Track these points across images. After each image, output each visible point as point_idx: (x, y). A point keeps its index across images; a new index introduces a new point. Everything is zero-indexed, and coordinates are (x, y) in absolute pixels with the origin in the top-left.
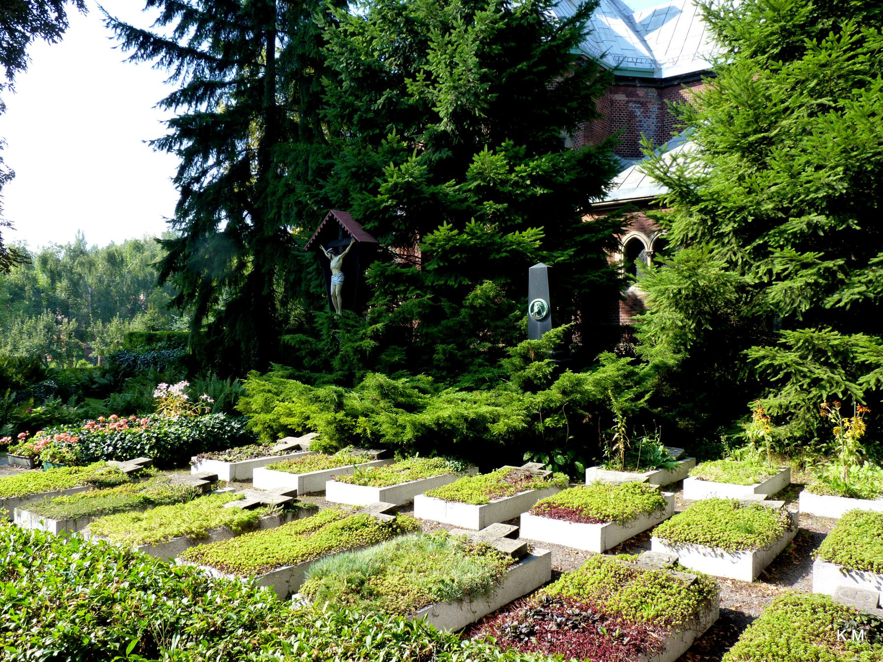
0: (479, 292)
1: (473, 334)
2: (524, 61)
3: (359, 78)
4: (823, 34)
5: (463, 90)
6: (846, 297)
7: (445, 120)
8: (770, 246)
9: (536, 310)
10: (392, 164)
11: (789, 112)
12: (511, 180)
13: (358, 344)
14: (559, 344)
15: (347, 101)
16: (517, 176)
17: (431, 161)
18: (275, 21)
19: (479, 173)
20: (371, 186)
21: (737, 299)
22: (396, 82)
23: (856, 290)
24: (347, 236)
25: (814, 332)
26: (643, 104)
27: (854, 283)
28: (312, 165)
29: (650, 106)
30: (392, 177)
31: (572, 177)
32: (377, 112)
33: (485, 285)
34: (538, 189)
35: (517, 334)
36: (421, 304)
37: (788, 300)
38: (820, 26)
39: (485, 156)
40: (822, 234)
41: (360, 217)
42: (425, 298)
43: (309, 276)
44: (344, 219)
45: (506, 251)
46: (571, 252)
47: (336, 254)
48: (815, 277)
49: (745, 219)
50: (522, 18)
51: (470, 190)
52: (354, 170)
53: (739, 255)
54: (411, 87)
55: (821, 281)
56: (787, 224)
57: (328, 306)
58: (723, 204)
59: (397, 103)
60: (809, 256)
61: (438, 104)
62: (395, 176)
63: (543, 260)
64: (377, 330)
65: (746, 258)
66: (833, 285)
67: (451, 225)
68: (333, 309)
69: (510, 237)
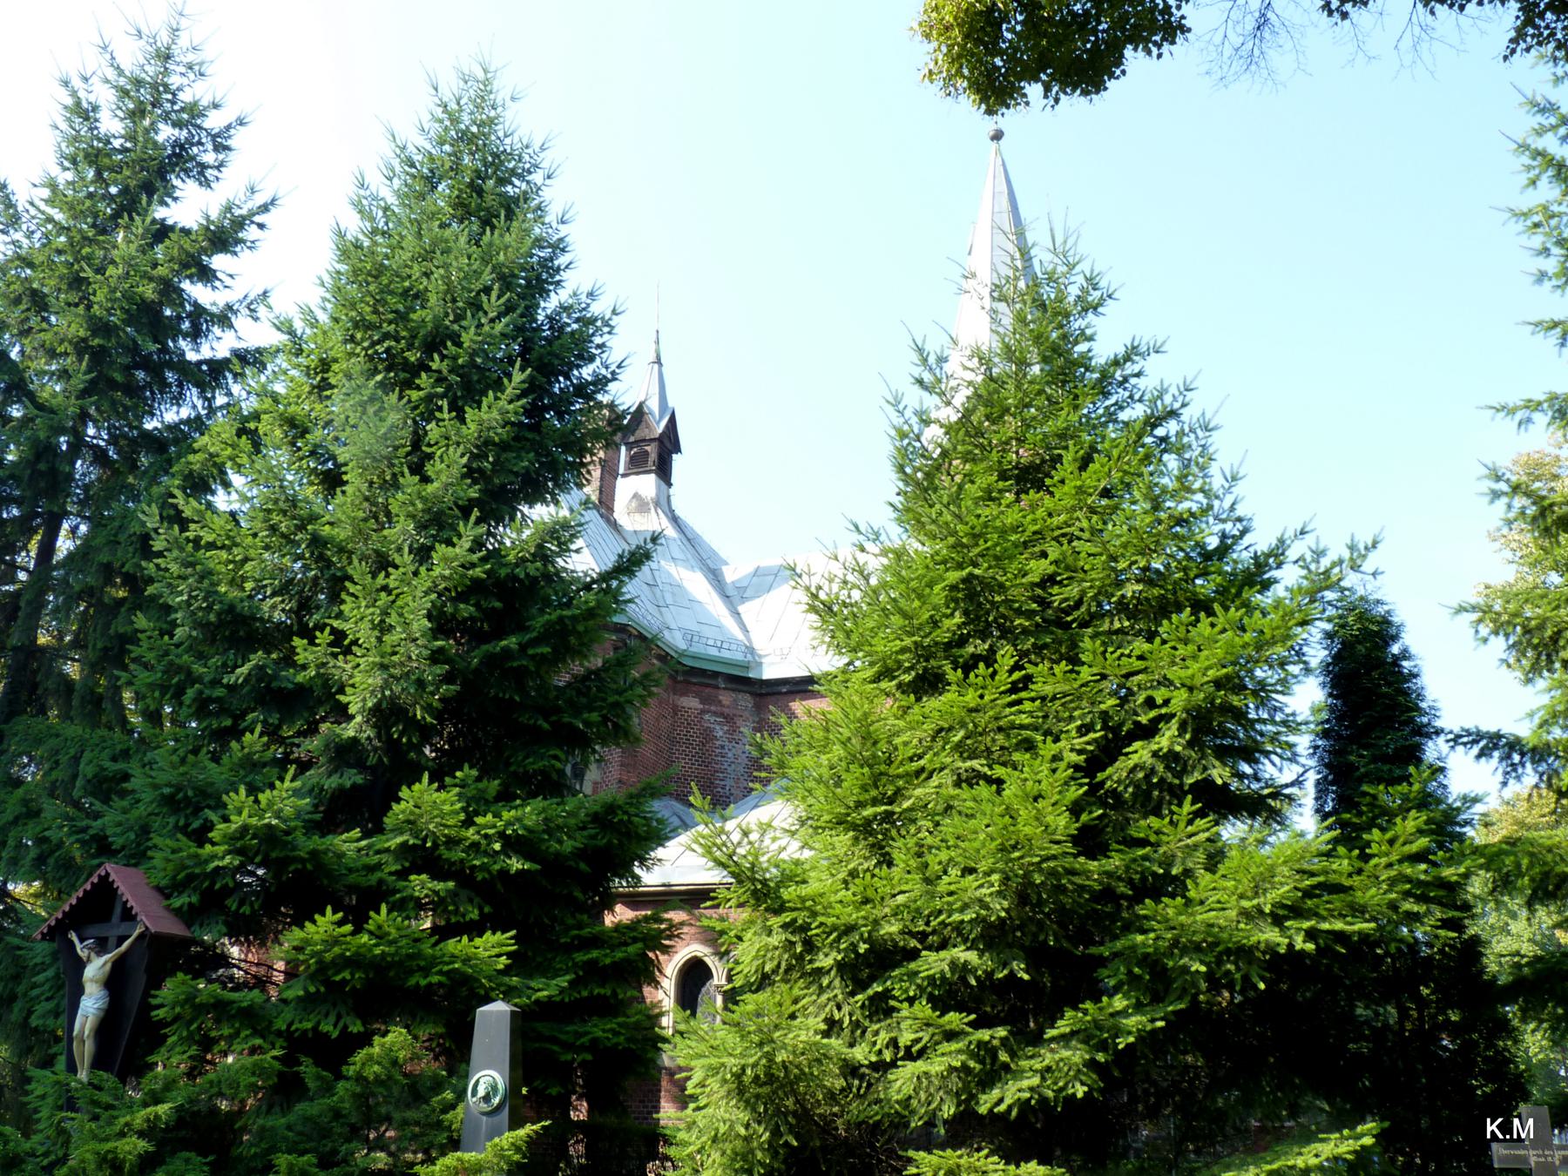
0: (376, 1050)
1: (355, 1133)
2: (513, 633)
3: (209, 624)
4: (968, 667)
5: (396, 672)
6: (1006, 1096)
7: (359, 719)
8: (894, 998)
9: (481, 1092)
10: (242, 790)
11: (924, 776)
12: (466, 839)
13: (110, 1145)
14: (518, 1164)
15: (177, 661)
16: (478, 833)
17: (322, 789)
18: (68, 495)
19: (409, 822)
20: (196, 824)
21: (842, 1090)
22: (277, 638)
23: (1025, 1083)
24: (128, 916)
25: (960, 1157)
26: (729, 719)
27: (1023, 1071)
28: (87, 770)
29: (739, 722)
30: (240, 813)
31: (578, 845)
32: (232, 688)
33: (389, 1038)
34: (514, 860)
35: (442, 1138)
36: (258, 1070)
37: (923, 1095)
38: (971, 649)
39: (422, 793)
40: (973, 982)
41: (164, 883)
42: (268, 1056)
43: (35, 992)
44: (130, 885)
45: (441, 973)
46: (563, 981)
47: (100, 954)
48: (963, 1057)
49: (854, 947)
50: (517, 565)
51: (387, 850)
52: (167, 791)
53: (846, 1009)
54: (303, 652)
55: (972, 1064)
56: (919, 962)
57: (62, 1059)
58: (821, 919)
59: (275, 677)
60: (954, 1019)
61: (349, 690)
62: (245, 813)
63: (508, 994)
64: (157, 1117)
65: (858, 1015)
66: (993, 1074)
67: (340, 915)
68: (72, 1068)
69: (452, 946)
